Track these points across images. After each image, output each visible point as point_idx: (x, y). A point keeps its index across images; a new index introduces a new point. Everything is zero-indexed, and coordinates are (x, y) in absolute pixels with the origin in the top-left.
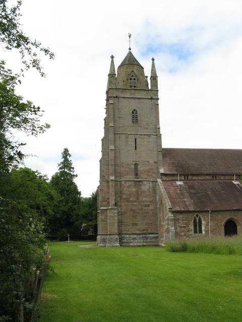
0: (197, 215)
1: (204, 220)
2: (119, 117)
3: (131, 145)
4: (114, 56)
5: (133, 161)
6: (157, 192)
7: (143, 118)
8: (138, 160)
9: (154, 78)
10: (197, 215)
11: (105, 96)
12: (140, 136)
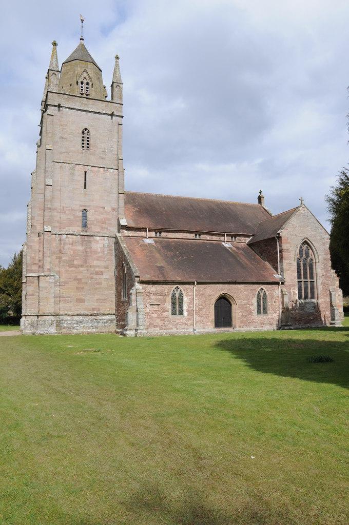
2: (61, 138)
5: (81, 206)
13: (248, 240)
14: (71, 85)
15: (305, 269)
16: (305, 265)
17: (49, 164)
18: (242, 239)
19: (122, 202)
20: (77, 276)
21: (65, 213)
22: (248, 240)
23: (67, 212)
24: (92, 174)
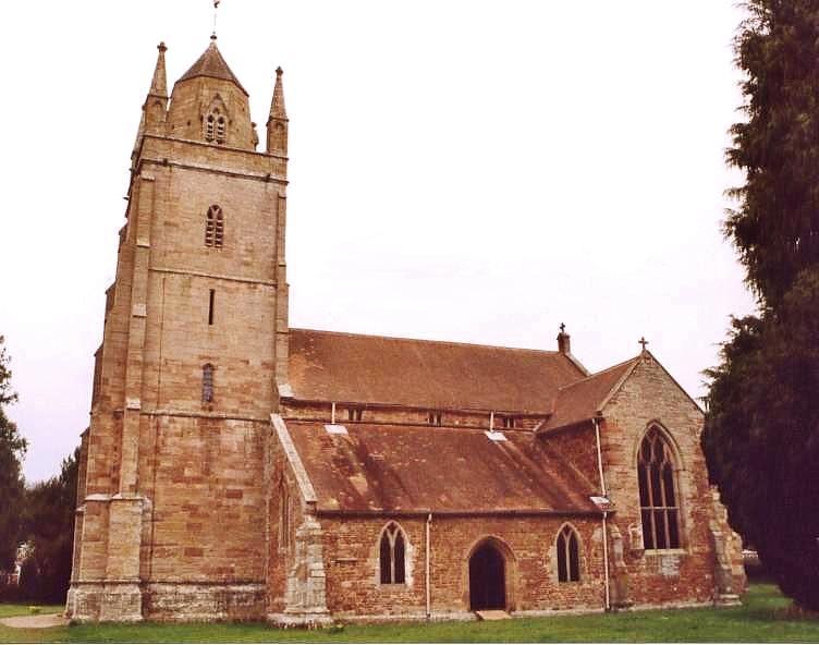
0: (392, 528)
1: (412, 543)
2: (166, 224)
5: (201, 358)
9: (278, 123)
10: (392, 528)
12: (228, 284)
21: (169, 371)
23: (174, 371)
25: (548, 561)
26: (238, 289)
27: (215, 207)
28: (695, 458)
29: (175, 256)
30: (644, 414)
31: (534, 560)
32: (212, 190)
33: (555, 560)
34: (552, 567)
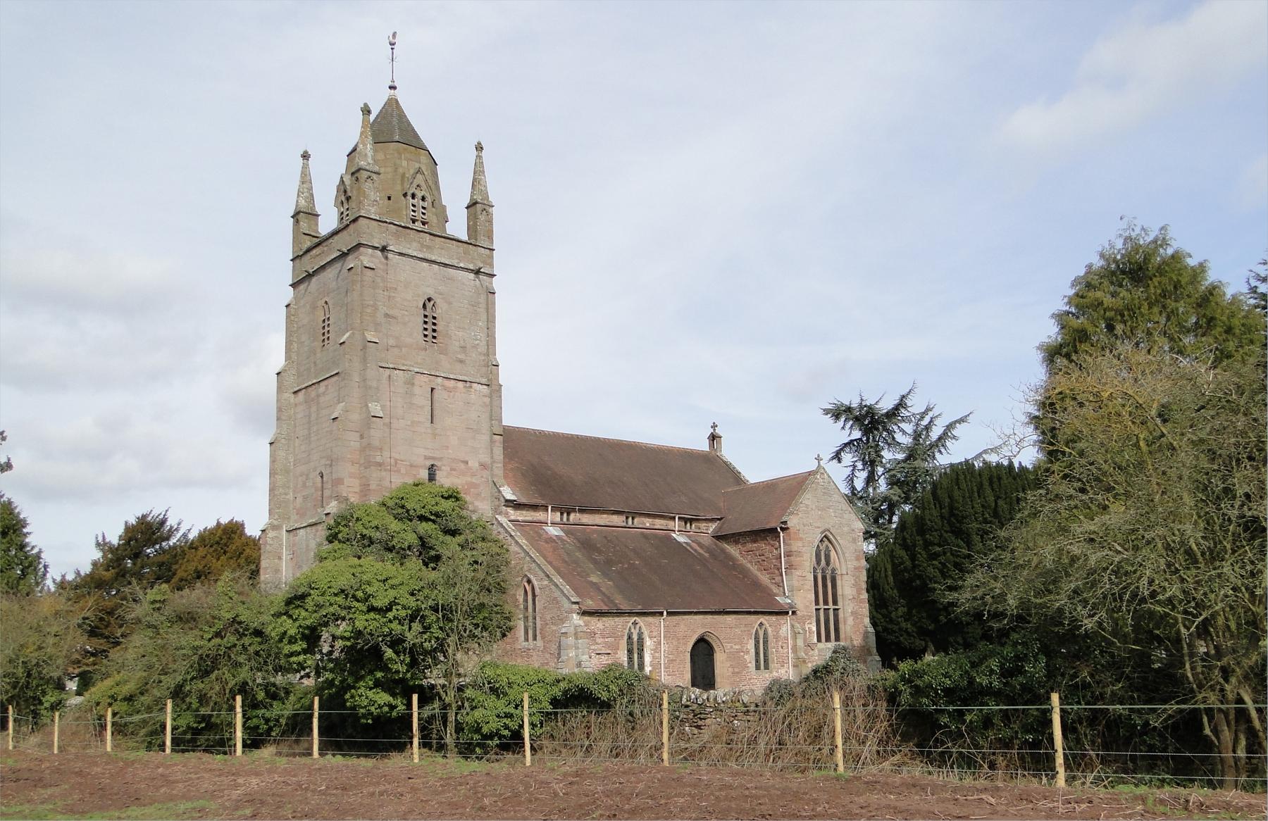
0: (635, 623)
1: (651, 637)
2: (387, 315)
3: (422, 407)
4: (13, 462)
5: (426, 458)
6: (31, 579)
7: (455, 330)
8: (437, 454)
9: (478, 207)
10: (635, 623)
11: (285, 272)
12: (447, 383)
13: (712, 527)
14: (389, 198)
15: (825, 586)
16: (824, 578)
17: (372, 372)
18: (703, 525)
19: (499, 452)
20: (207, 594)
21: (398, 471)
22: (712, 527)
23: (403, 471)
24: (445, 394)
25: (748, 652)
26: (455, 388)
27: (429, 300)
28: (856, 564)
29: (396, 350)
30: (819, 524)
31: (738, 651)
32: (424, 281)
33: (753, 651)
34: (750, 658)
